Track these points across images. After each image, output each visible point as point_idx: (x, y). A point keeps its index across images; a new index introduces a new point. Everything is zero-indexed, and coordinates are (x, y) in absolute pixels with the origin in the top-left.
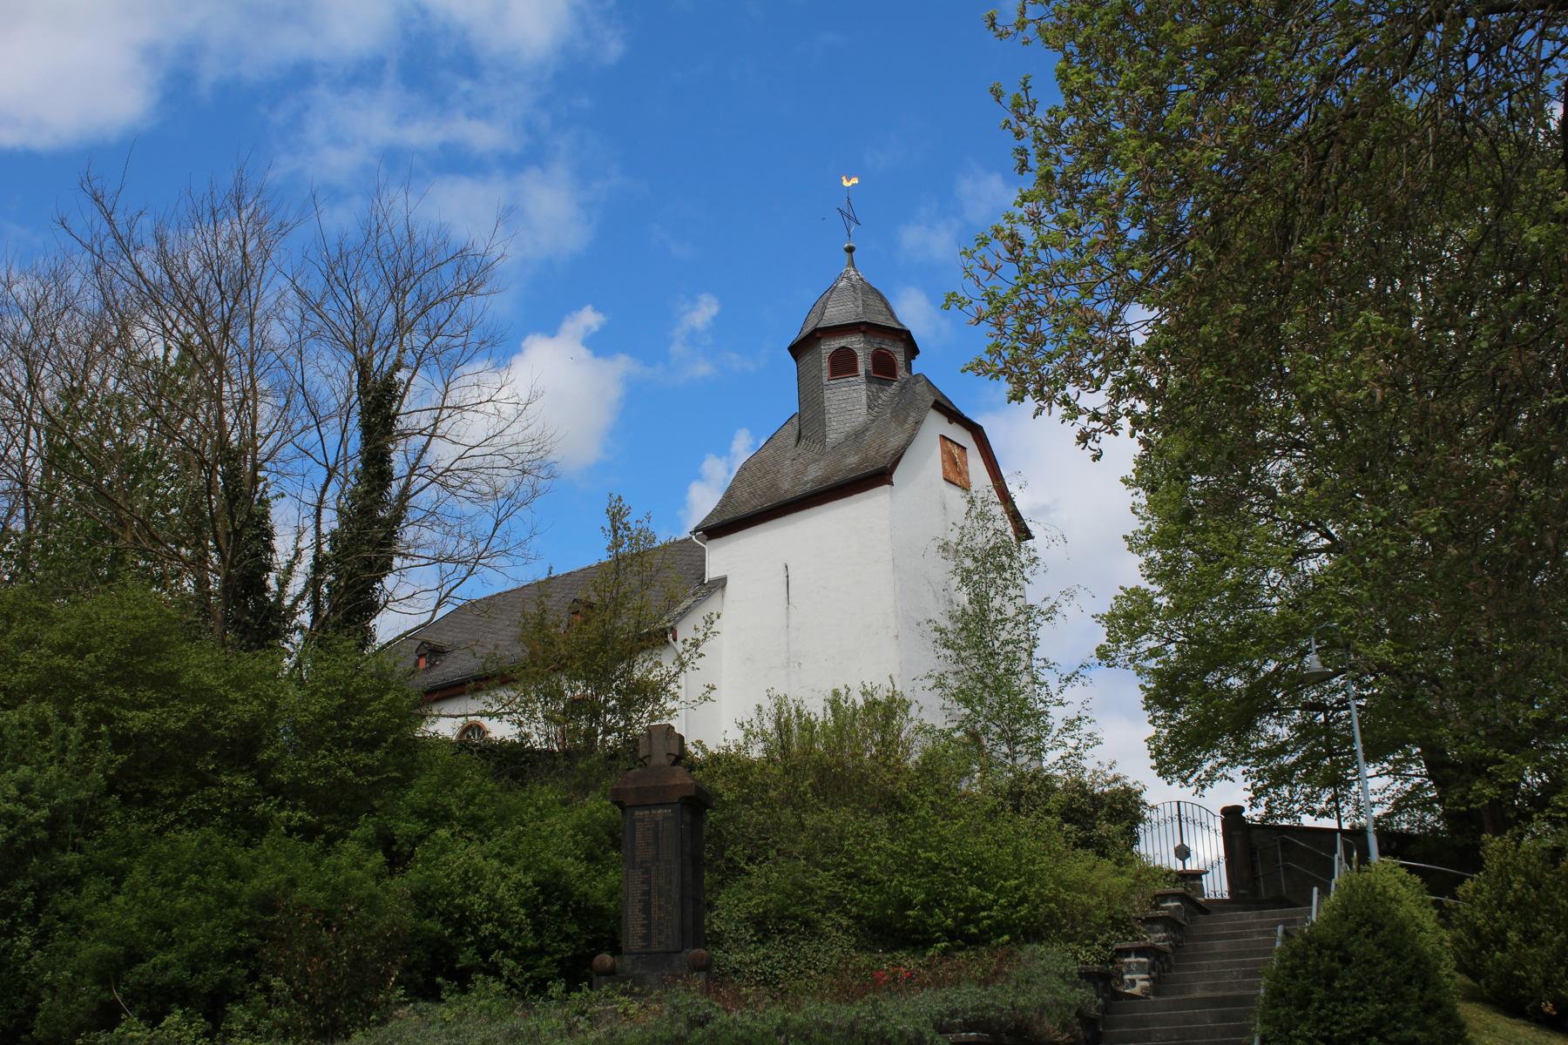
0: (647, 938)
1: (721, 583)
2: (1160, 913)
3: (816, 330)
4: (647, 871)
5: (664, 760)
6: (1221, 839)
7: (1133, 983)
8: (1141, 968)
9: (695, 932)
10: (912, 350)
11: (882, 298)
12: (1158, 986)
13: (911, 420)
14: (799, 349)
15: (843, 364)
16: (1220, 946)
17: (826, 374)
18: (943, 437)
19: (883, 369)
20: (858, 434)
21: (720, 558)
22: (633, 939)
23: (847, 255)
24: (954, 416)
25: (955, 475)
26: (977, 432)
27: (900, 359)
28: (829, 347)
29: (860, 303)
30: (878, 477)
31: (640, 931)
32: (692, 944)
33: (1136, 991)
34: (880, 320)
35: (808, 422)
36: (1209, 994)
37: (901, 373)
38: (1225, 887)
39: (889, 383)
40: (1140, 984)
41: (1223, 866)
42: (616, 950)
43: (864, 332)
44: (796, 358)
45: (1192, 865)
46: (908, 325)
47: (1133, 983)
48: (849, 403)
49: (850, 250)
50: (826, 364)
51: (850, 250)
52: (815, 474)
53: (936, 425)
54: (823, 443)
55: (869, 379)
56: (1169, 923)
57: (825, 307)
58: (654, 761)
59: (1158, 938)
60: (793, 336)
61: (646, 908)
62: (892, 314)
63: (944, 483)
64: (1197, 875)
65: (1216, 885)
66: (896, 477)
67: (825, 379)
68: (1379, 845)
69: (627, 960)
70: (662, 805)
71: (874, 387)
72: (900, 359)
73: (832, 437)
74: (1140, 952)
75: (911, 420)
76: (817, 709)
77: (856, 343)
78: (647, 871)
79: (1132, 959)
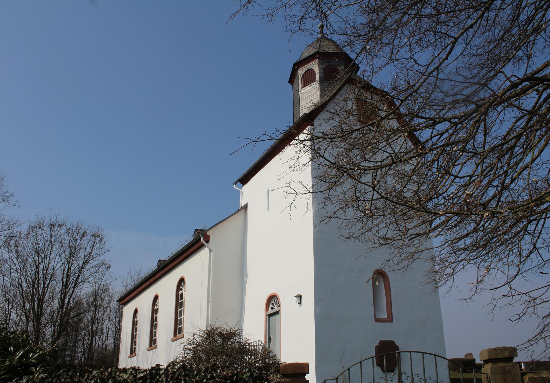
15: (308, 79)
21: (249, 193)
28: (301, 72)
34: (331, 49)
66: (316, 122)
67: (300, 88)
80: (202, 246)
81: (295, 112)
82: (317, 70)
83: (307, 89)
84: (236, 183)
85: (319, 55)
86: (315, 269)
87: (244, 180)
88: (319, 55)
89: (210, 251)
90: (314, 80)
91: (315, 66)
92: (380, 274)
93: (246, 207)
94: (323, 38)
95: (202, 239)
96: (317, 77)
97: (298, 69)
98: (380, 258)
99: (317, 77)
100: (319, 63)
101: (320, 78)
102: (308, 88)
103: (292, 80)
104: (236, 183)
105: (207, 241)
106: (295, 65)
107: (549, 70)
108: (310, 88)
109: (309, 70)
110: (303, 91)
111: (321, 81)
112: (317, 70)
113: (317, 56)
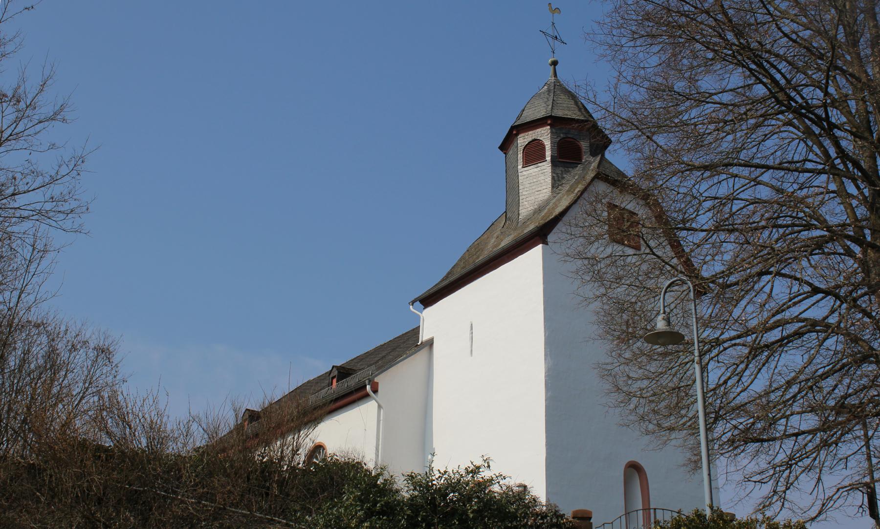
1: (430, 343)
15: (534, 154)
21: (434, 321)
28: (523, 140)
34: (572, 113)
39: (574, 165)
50: (520, 156)
51: (555, 63)
66: (551, 238)
67: (520, 167)
77: (544, 135)
80: (367, 395)
81: (510, 200)
82: (548, 144)
83: (531, 171)
84: (413, 303)
85: (553, 121)
86: (547, 449)
87: (429, 300)
88: (553, 121)
89: (380, 407)
90: (541, 158)
91: (544, 135)
92: (634, 468)
93: (430, 343)
94: (558, 88)
95: (368, 387)
96: (548, 154)
97: (517, 135)
98: (638, 446)
99: (548, 154)
100: (552, 133)
101: (552, 156)
102: (532, 170)
103: (505, 146)
104: (413, 303)
105: (375, 391)
106: (513, 128)
107: (879, 466)
108: (536, 170)
109: (535, 140)
110: (525, 173)
111: (554, 163)
112: (548, 144)
113: (549, 122)
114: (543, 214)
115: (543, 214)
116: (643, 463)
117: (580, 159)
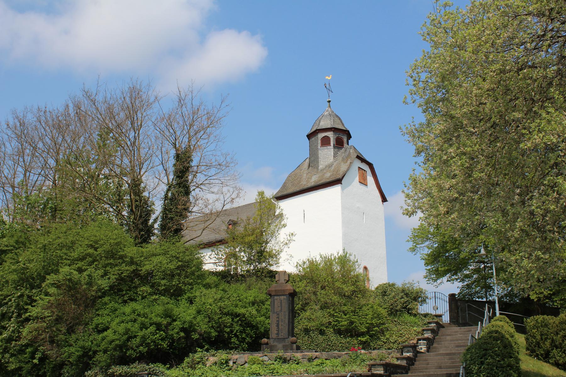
0: (278, 334)
2: (430, 328)
3: (317, 130)
4: (278, 314)
5: (283, 282)
6: (448, 304)
7: (421, 348)
8: (424, 344)
9: (292, 333)
10: (349, 137)
11: (340, 119)
12: (428, 351)
13: (349, 162)
14: (309, 136)
15: (325, 142)
16: (448, 338)
17: (319, 145)
18: (359, 168)
19: (339, 144)
20: (330, 166)
21: (285, 206)
22: (273, 333)
23: (328, 103)
24: (363, 160)
25: (363, 182)
26: (370, 165)
27: (345, 140)
28: (321, 135)
29: (332, 121)
30: (338, 181)
31: (276, 332)
32: (293, 338)
33: (422, 351)
35: (313, 161)
36: (445, 352)
37: (345, 145)
38: (449, 319)
39: (341, 148)
40: (423, 349)
41: (448, 312)
42: (268, 338)
43: (333, 131)
44: (309, 139)
45: (439, 312)
46: (348, 129)
47: (421, 348)
48: (327, 155)
49: (329, 102)
50: (319, 142)
52: (314, 180)
53: (358, 164)
54: (317, 168)
55: (335, 147)
56: (433, 331)
57: (320, 122)
58: (280, 282)
59: (428, 335)
60: (308, 131)
61: (278, 326)
62: (343, 124)
63: (359, 183)
64: (440, 316)
65: (446, 319)
67: (319, 147)
68: (499, 306)
69: (272, 340)
70: (283, 295)
71: (336, 150)
72: (345, 140)
73: (321, 167)
74: (424, 339)
75: (349, 162)
76: (318, 259)
77: (330, 134)
78: (278, 314)
79: (421, 341)
87: (281, 198)
99: (332, 145)
114: (333, 168)
115: (333, 168)
116: (368, 266)
117: (343, 145)
